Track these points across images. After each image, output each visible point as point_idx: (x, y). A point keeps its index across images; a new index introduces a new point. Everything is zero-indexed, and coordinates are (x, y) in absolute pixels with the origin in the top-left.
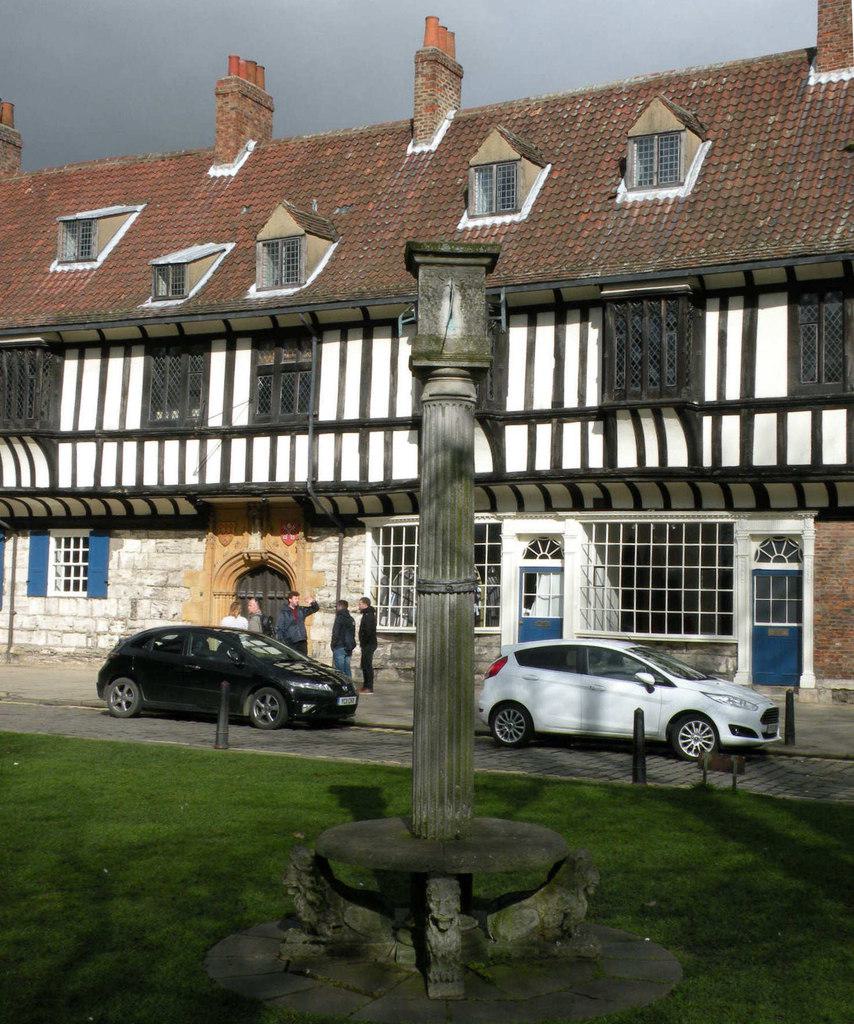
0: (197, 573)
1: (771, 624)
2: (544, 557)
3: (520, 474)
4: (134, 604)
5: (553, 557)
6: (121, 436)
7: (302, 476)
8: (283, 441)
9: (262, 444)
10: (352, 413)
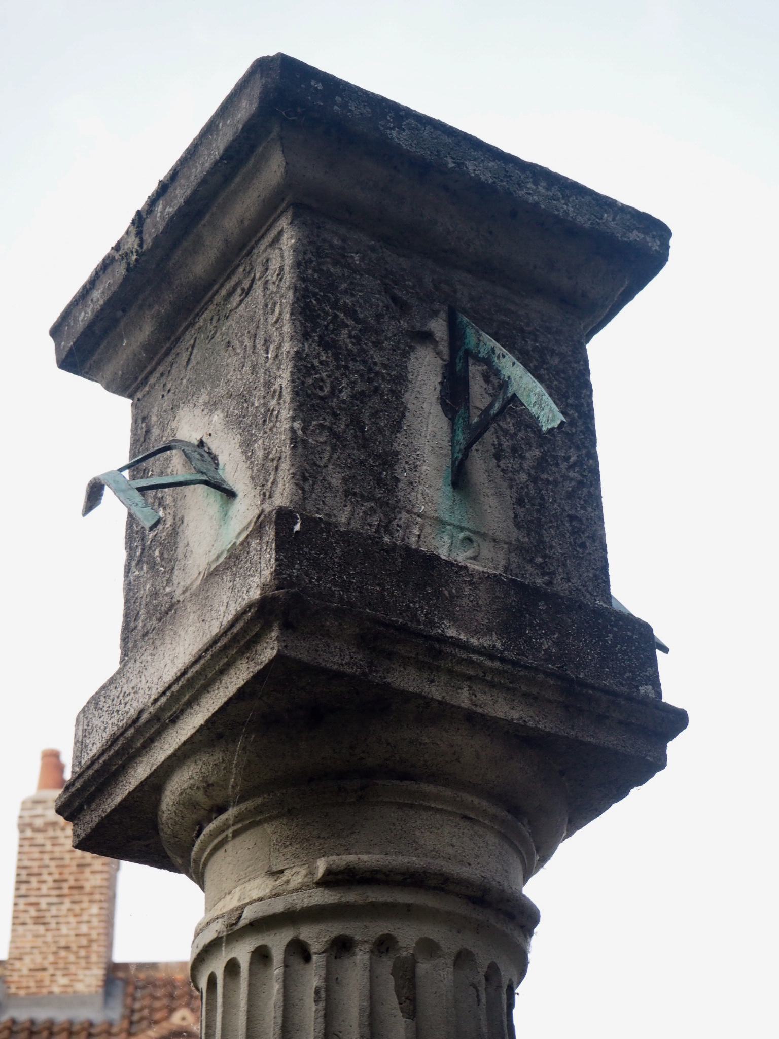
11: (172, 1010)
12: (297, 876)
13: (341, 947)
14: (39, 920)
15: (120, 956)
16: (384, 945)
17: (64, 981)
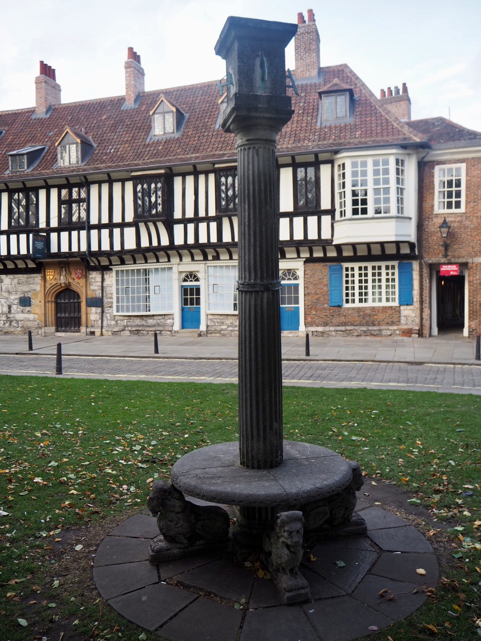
0: (38, 293)
1: (301, 305)
2: (191, 281)
3: (181, 246)
4: (10, 307)
5: (195, 281)
6: (207, 219)
7: (84, 248)
8: (74, 234)
9: (64, 235)
10: (105, 220)
11: (334, 78)
12: (244, 140)
13: (249, 148)
14: (301, 59)
15: (323, 64)
16: (254, 148)
17: (308, 73)
